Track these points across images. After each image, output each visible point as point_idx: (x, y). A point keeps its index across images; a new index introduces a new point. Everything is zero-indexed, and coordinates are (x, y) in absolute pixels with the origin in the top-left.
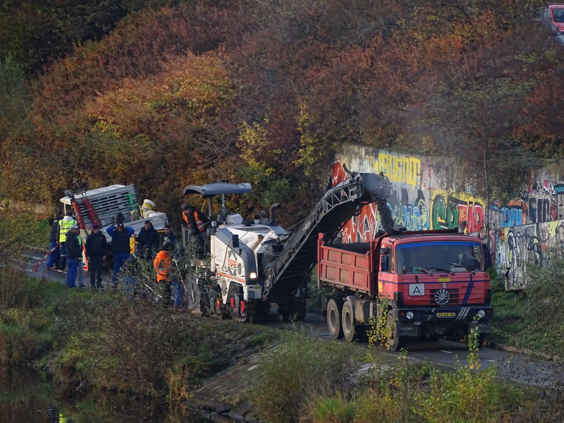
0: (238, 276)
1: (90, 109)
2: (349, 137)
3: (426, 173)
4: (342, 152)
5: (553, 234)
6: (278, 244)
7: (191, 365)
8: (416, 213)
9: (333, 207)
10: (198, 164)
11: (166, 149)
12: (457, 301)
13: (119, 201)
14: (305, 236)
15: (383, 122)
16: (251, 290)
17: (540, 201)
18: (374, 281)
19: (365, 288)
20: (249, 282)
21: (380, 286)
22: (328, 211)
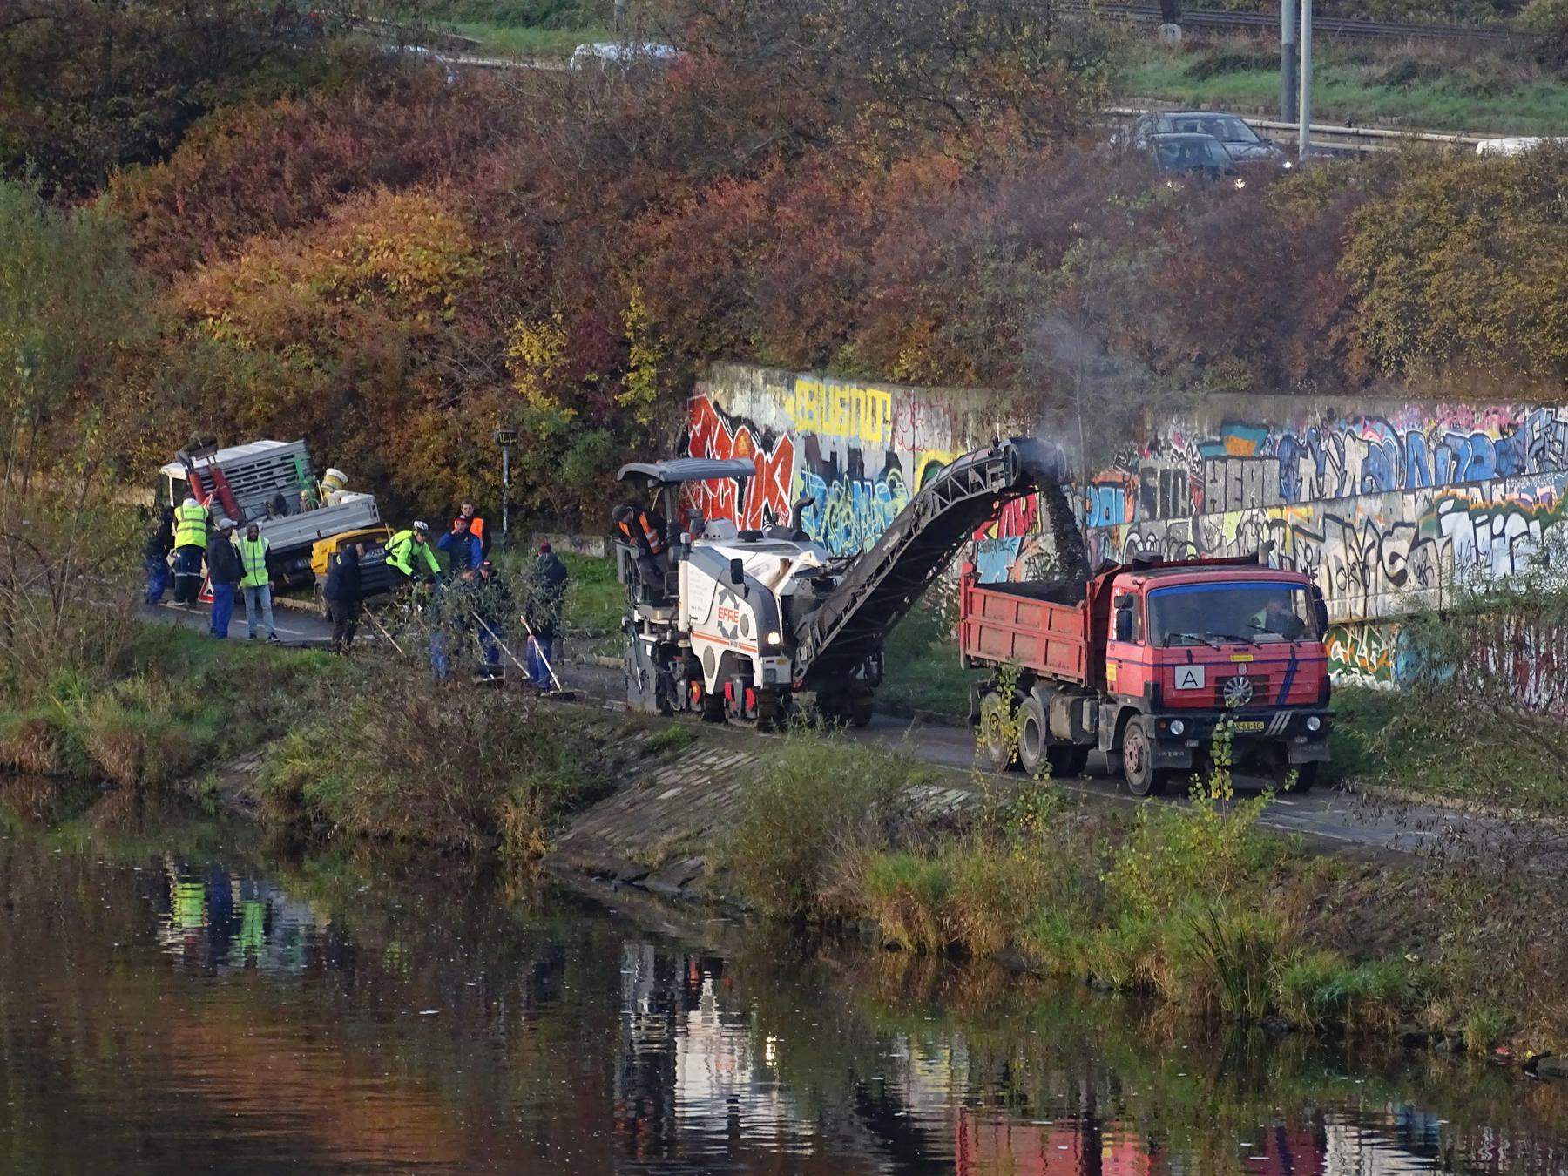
0: (741, 639)
1: (186, 294)
2: (727, 351)
3: (905, 420)
4: (710, 378)
5: (1231, 537)
6: (822, 577)
7: (547, 789)
8: (883, 496)
9: (950, 504)
10: (425, 401)
11: (359, 374)
12: (1266, 698)
13: (277, 472)
14: (887, 561)
15: (808, 322)
16: (770, 666)
17: (1165, 473)
18: (1096, 657)
19: (1076, 672)
20: (766, 650)
21: (1111, 671)
22: (939, 512)
